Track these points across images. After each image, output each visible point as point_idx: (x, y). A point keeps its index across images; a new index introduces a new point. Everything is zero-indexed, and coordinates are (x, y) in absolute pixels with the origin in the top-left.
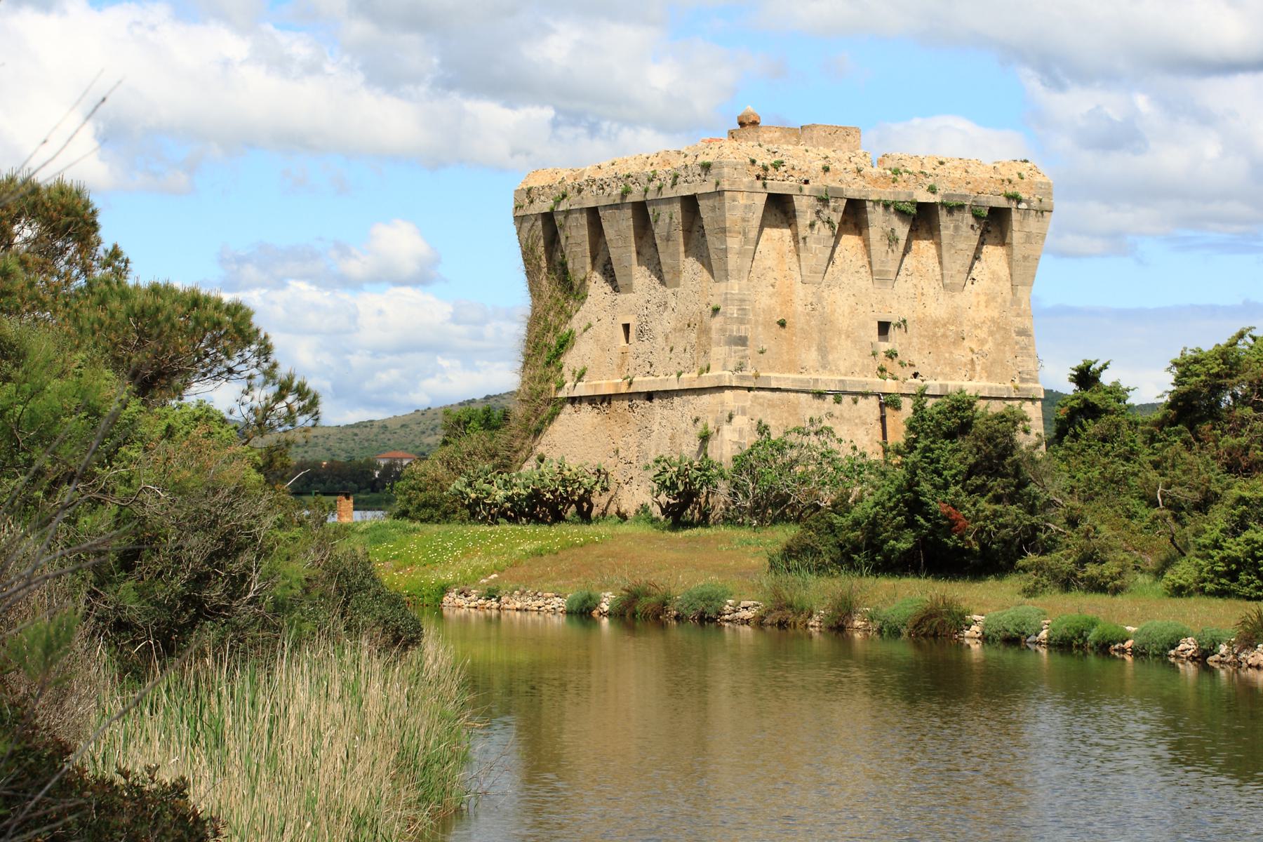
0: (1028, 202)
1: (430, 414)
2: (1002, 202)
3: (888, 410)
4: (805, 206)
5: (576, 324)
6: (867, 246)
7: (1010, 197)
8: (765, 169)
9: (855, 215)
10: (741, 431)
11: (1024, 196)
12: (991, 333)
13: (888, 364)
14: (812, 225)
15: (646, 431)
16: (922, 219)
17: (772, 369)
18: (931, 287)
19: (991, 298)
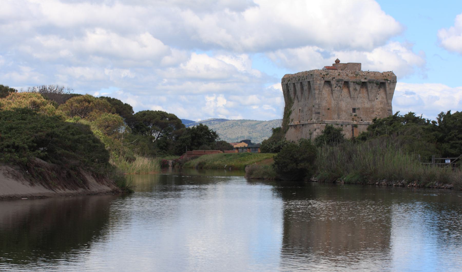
0: (390, 81)
1: (259, 128)
2: (383, 81)
3: (354, 128)
4: (333, 82)
5: (292, 109)
6: (349, 90)
7: (385, 80)
8: (324, 75)
9: (346, 83)
10: (318, 133)
11: (389, 79)
12: (381, 111)
13: (355, 118)
14: (336, 87)
15: (302, 132)
16: (363, 85)
17: (326, 119)
18: (366, 101)
19: (381, 103)
